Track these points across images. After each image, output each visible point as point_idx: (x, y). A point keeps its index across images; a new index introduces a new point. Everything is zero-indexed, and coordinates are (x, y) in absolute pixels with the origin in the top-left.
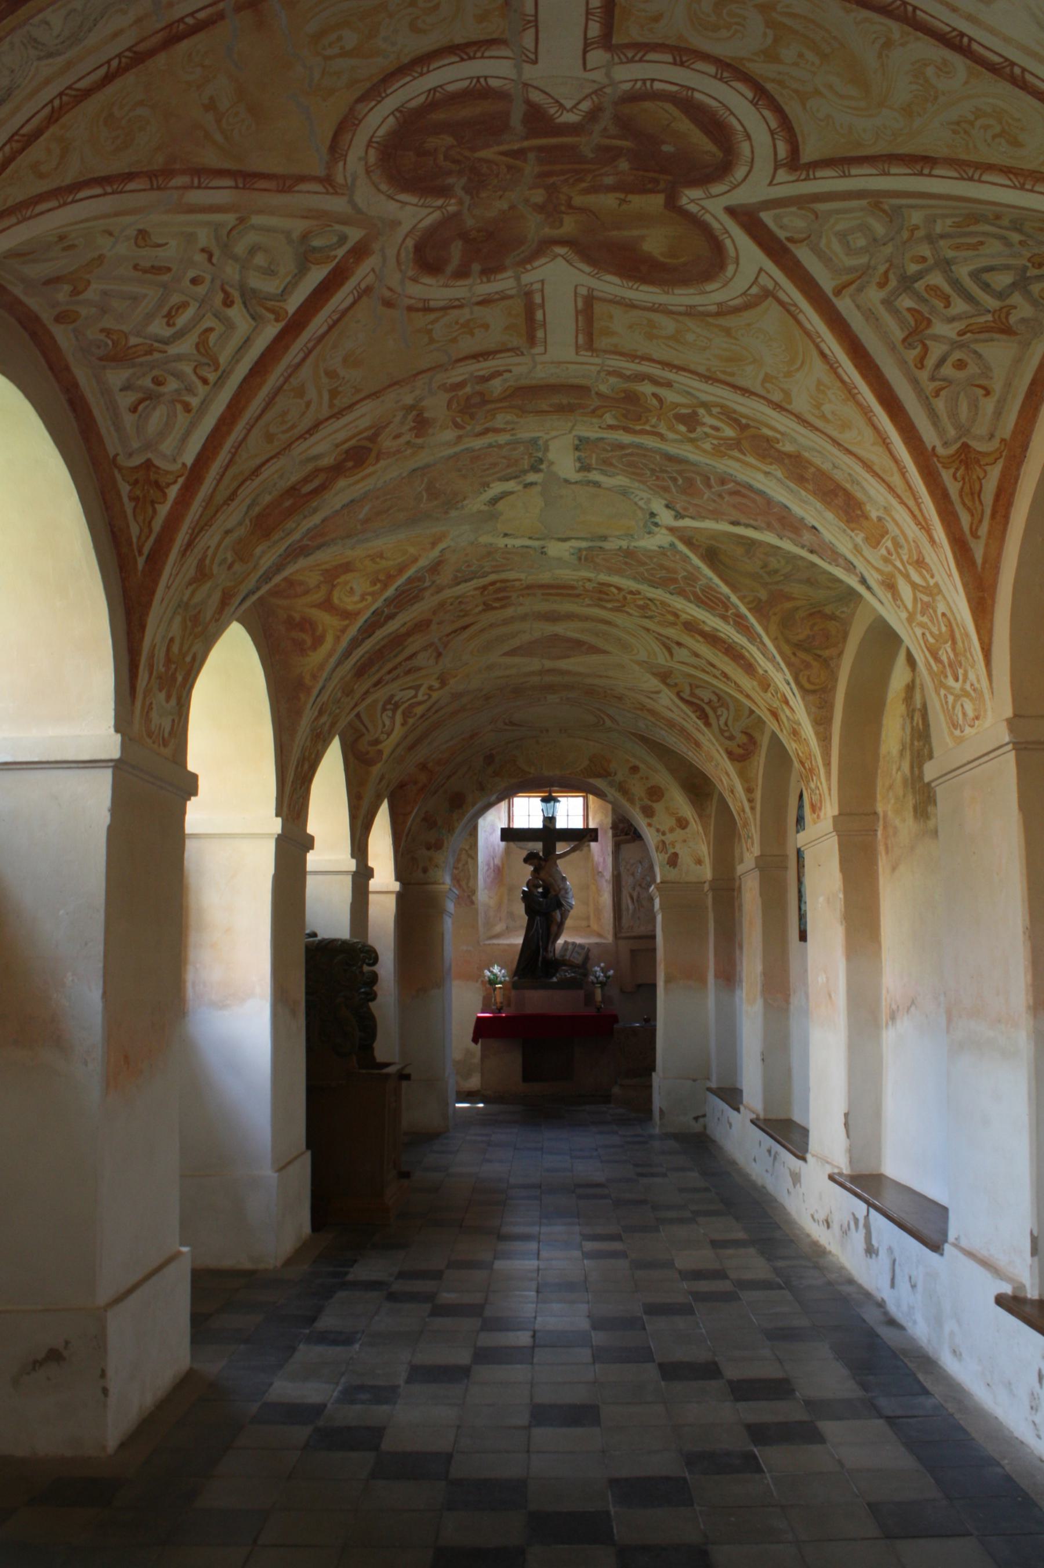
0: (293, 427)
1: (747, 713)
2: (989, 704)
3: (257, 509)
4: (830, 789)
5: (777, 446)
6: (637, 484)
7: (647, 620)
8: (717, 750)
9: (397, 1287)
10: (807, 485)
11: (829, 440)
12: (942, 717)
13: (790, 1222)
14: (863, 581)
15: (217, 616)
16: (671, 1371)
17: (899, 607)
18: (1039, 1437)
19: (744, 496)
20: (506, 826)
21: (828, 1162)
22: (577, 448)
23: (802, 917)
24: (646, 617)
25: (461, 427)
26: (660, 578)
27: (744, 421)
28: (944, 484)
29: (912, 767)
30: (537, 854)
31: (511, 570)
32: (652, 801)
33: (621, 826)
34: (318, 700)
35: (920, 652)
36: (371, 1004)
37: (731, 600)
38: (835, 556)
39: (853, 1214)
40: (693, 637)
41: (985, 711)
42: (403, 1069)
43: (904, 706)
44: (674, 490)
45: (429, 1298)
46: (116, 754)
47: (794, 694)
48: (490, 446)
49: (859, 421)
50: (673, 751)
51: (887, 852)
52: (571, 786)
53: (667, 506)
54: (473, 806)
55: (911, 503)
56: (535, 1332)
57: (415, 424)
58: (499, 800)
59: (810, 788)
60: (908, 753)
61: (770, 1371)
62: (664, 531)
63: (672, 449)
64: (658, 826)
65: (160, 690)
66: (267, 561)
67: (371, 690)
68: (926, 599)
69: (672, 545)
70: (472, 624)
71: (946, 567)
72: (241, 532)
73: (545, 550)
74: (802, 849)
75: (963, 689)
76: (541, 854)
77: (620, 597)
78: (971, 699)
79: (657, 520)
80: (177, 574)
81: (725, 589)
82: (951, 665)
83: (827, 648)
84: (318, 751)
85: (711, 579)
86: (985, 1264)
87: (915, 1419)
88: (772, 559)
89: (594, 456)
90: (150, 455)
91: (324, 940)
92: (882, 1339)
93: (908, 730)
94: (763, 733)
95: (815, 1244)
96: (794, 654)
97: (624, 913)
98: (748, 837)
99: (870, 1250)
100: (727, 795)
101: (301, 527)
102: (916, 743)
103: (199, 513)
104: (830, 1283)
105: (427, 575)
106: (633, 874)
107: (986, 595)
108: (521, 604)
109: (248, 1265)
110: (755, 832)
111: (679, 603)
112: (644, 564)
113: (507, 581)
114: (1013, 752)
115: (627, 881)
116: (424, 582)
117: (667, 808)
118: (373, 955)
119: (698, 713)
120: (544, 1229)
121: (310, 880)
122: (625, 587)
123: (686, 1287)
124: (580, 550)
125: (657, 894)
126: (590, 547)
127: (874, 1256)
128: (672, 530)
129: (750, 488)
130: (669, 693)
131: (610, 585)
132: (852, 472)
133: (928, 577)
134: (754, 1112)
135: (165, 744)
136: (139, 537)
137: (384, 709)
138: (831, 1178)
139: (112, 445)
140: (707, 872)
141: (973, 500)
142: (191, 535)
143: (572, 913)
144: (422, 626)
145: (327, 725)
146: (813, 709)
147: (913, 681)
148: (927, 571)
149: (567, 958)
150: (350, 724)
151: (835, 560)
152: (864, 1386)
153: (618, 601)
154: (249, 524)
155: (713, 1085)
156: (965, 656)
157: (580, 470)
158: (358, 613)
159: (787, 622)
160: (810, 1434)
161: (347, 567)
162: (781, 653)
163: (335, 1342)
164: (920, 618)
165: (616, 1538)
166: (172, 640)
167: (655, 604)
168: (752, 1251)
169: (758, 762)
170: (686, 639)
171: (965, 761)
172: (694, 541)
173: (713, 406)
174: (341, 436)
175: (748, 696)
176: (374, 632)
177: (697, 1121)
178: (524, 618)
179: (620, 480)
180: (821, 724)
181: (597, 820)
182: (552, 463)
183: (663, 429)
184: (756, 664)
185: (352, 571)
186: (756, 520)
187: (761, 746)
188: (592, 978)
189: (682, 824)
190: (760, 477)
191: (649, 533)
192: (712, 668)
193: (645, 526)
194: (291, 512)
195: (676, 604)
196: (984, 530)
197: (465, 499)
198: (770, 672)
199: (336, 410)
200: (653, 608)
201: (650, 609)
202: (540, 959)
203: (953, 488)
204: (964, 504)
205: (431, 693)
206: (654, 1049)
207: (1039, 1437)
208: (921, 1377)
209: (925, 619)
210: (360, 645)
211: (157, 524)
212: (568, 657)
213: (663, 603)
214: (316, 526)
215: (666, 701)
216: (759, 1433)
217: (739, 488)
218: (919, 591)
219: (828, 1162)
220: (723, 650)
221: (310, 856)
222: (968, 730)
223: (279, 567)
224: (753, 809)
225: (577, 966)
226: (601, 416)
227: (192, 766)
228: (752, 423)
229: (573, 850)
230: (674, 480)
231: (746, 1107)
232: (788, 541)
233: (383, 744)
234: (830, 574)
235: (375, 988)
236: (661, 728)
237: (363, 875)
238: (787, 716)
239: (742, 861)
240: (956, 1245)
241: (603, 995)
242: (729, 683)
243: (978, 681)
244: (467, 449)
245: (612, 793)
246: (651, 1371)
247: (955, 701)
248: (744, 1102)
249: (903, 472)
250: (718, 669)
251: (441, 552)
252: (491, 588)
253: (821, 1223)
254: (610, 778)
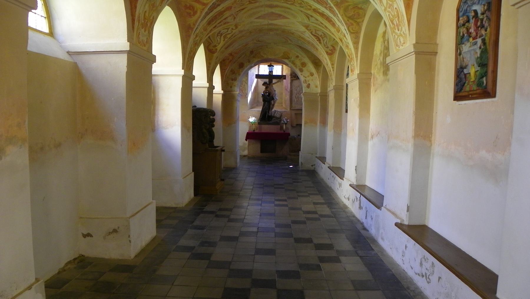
1: (333, 40)
2: (408, 39)
4: (357, 65)
7: (301, 8)
8: (323, 51)
9: (218, 213)
13: (338, 198)
15: (160, 4)
16: (298, 240)
17: (382, 6)
18: (404, 264)
20: (257, 74)
21: (349, 181)
24: (301, 7)
30: (267, 83)
33: (293, 75)
34: (195, 32)
35: (388, 21)
37: (328, 2)
39: (356, 197)
40: (316, 14)
43: (382, 39)
46: (128, 49)
50: (309, 51)
51: (374, 86)
54: (246, 67)
56: (258, 227)
58: (255, 65)
60: (382, 54)
61: (327, 242)
65: (142, 28)
67: (213, 29)
68: (390, 3)
74: (348, 84)
75: (400, 34)
82: (397, 25)
83: (359, 19)
86: (393, 213)
87: (368, 257)
91: (198, 108)
92: (361, 234)
93: (383, 47)
94: (338, 47)
95: (345, 205)
96: (348, 20)
98: (332, 79)
99: (360, 208)
100: (326, 66)
102: (385, 51)
104: (348, 216)
109: (174, 206)
110: (334, 77)
114: (415, 55)
115: (295, 92)
118: (214, 113)
119: (317, 39)
120: (263, 197)
121: (194, 90)
123: (304, 216)
125: (303, 96)
134: (329, 165)
135: (145, 46)
137: (218, 36)
138: (350, 185)
140: (319, 90)
143: (277, 101)
144: (229, 8)
147: (386, 31)
149: (275, 115)
152: (355, 247)
155: (318, 156)
156: (402, 22)
159: (346, 10)
160: (338, 261)
163: (199, 229)
164: (388, 9)
165: (277, 287)
166: (146, 12)
167: (304, 3)
168: (325, 206)
171: (399, 57)
175: (333, 34)
176: (213, 10)
177: (312, 166)
178: (262, 6)
180: (355, 44)
181: (286, 72)
184: (336, 23)
188: (282, 122)
192: (321, 24)
200: (304, 4)
201: (302, 5)
202: (267, 115)
205: (233, 30)
206: (300, 144)
207: (404, 264)
208: (371, 245)
210: (209, 14)
212: (276, 19)
215: (308, 35)
216: (322, 259)
219: (349, 181)
220: (326, 19)
221: (194, 82)
222: (401, 47)
224: (333, 70)
225: (278, 118)
227: (154, 53)
229: (278, 82)
231: (327, 163)
233: (218, 47)
237: (211, 88)
238: (345, 41)
239: (329, 87)
240: (385, 208)
241: (286, 127)
243: (405, 31)
246: (292, 240)
247: (398, 37)
248: (327, 161)
250: (324, 25)
254: (290, 59)
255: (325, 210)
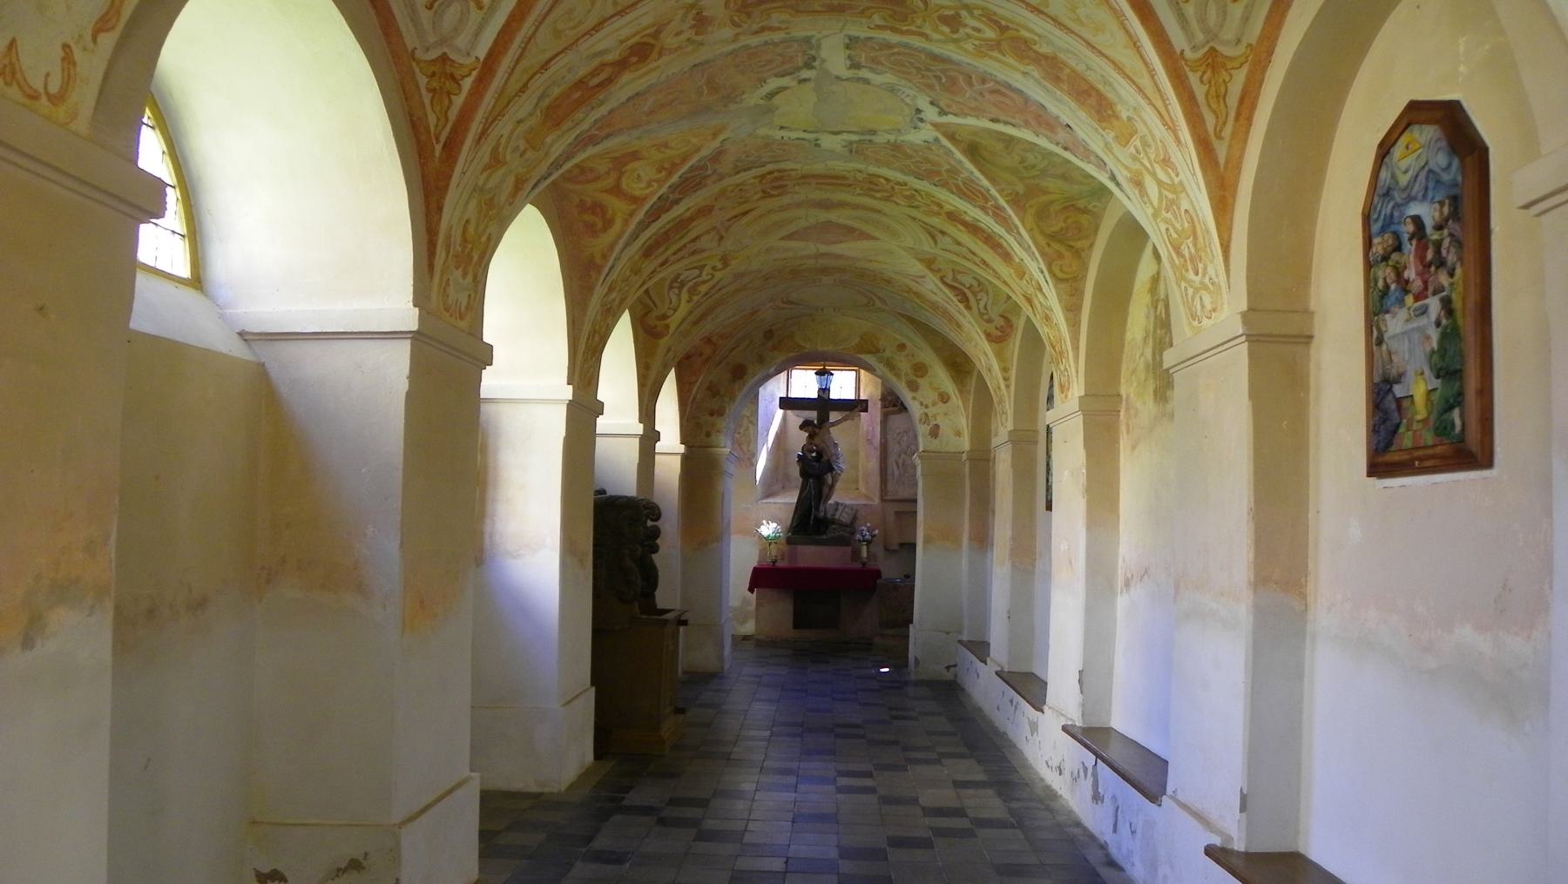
0: (580, 23)
3: (547, 101)
4: (1077, 372)
5: (1034, 47)
6: (903, 82)
8: (977, 332)
10: (1062, 85)
11: (1083, 43)
12: (1181, 308)
14: (1113, 178)
15: (511, 200)
17: (1145, 203)
19: (1004, 95)
21: (1063, 715)
22: (848, 47)
23: (1049, 489)
25: (739, 26)
26: (924, 171)
27: (1003, 23)
28: (1191, 87)
29: (1154, 354)
31: (789, 160)
32: (917, 376)
33: (889, 398)
35: (1164, 246)
36: (653, 556)
38: (1087, 154)
39: (1083, 763)
40: (955, 226)
41: (1222, 304)
42: (680, 615)
44: (938, 87)
45: (696, 823)
47: (1047, 282)
48: (766, 43)
49: (1113, 26)
51: (1128, 432)
52: (845, 362)
53: (932, 103)
54: (754, 376)
55: (1159, 104)
57: (695, 22)
59: (1060, 370)
61: (954, 804)
62: (929, 126)
63: (937, 49)
64: (922, 400)
65: (457, 268)
66: (558, 149)
67: (658, 270)
68: (1170, 196)
69: (936, 139)
70: (752, 210)
71: (1189, 162)
72: (533, 122)
73: (818, 142)
75: (1202, 282)
76: (816, 422)
77: (888, 187)
78: (1210, 293)
79: (922, 116)
80: (472, 161)
81: (985, 182)
83: (1079, 239)
84: (608, 325)
85: (972, 173)
86: (1198, 816)
88: (1029, 154)
89: (863, 55)
90: (446, 50)
91: (611, 497)
93: (1152, 319)
95: (1048, 788)
96: (1049, 245)
97: (890, 478)
99: (1097, 797)
101: (587, 120)
102: (1159, 332)
103: (492, 104)
105: (709, 164)
106: (899, 443)
107: (1227, 194)
108: (797, 193)
109: (534, 789)
110: (1009, 408)
111: (943, 195)
112: (911, 157)
113: (785, 171)
115: (894, 448)
116: (707, 170)
117: (931, 384)
122: (892, 178)
124: (851, 143)
125: (919, 461)
126: (860, 140)
127: (1099, 802)
128: (935, 125)
129: (1009, 86)
130: (934, 278)
131: (879, 176)
132: (1103, 73)
133: (1173, 175)
134: (999, 665)
136: (437, 126)
137: (671, 288)
138: (1065, 729)
139: (411, 40)
140: (965, 444)
141: (1219, 101)
142: (485, 124)
143: (843, 476)
144: (705, 211)
145: (618, 300)
146: (1064, 297)
147: (1158, 273)
148: (1173, 170)
149: (837, 517)
150: (639, 300)
151: (1088, 157)
153: (886, 191)
154: (539, 115)
155: (965, 638)
157: (850, 68)
158: (644, 199)
159: (1042, 214)
161: (635, 156)
162: (1035, 243)
166: (468, 221)
168: (990, 792)
169: (1014, 343)
170: (950, 228)
172: (957, 137)
173: (975, 9)
174: (625, 33)
175: (1005, 283)
176: (659, 217)
177: (948, 671)
178: (799, 205)
179: (889, 78)
181: (867, 393)
182: (824, 61)
183: (928, 31)
184: (1012, 253)
185: (639, 159)
186: (1014, 118)
187: (1017, 329)
188: (858, 536)
189: (944, 398)
190: (1019, 76)
191: (915, 128)
192: (972, 255)
193: (912, 121)
194: (579, 103)
195: (940, 195)
196: (1227, 131)
197: (743, 93)
198: (1026, 261)
199: (619, 8)
200: (919, 199)
201: (916, 200)
202: (812, 517)
203: (1200, 91)
204: (1209, 106)
205: (715, 273)
209: (1169, 215)
210: (647, 228)
211: (453, 114)
213: (928, 194)
214: (603, 117)
215: (931, 286)
217: (1000, 88)
218: (1164, 188)
221: (600, 420)
222: (1205, 321)
223: (568, 155)
224: (1008, 387)
225: (847, 526)
226: (870, 17)
227: (487, 338)
228: (1011, 25)
229: (844, 419)
230: (938, 78)
231: (992, 660)
232: (1044, 138)
234: (1083, 170)
235: (658, 541)
236: (927, 310)
237: (650, 438)
239: (996, 435)
240: (1171, 797)
241: (868, 552)
242: (988, 270)
243: (1217, 276)
244: (743, 46)
245: (880, 367)
248: (991, 655)
249: (1152, 74)
251: (721, 142)
252: (769, 176)
253: (1054, 769)
255: (989, 804)
